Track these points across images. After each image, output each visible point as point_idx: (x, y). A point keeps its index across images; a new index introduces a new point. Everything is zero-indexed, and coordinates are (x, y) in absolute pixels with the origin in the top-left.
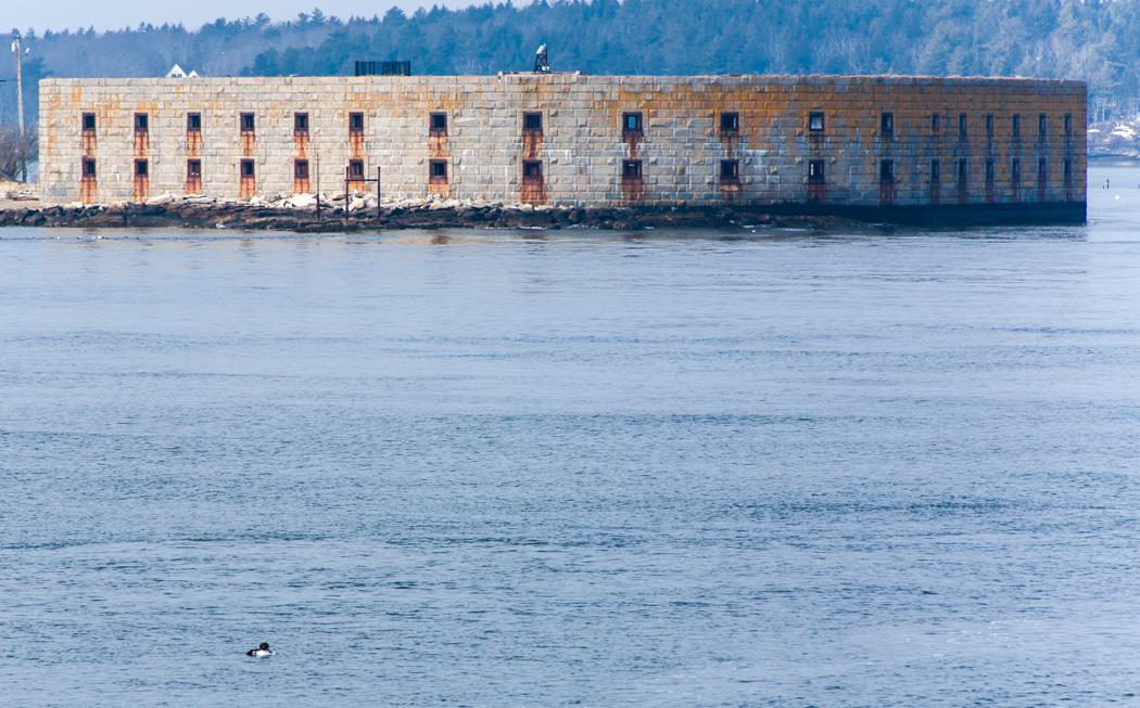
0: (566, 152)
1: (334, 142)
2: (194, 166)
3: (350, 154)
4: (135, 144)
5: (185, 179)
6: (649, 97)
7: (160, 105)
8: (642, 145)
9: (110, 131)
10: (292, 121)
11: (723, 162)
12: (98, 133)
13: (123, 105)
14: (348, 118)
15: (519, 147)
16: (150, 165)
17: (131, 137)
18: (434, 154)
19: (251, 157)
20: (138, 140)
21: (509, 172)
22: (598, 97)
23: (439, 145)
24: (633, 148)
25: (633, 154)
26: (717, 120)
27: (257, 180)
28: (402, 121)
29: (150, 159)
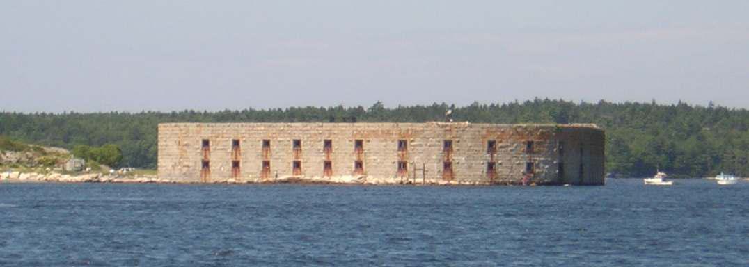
1: (346, 153)
2: (266, 164)
3: (355, 158)
5: (261, 169)
8: (495, 155)
9: (218, 148)
10: (322, 143)
11: (489, 163)
13: (225, 136)
17: (230, 150)
19: (299, 160)
20: (234, 152)
21: (436, 166)
25: (492, 159)
28: (384, 143)
29: (241, 161)
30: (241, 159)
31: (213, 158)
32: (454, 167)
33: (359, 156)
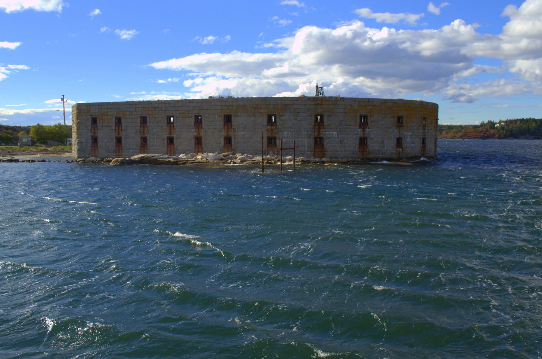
0: (334, 133)
3: (224, 134)
4: (115, 130)
6: (371, 108)
7: (127, 113)
8: (367, 130)
12: (98, 126)
14: (223, 117)
15: (312, 131)
16: (123, 139)
17: (114, 127)
18: (269, 134)
20: (117, 128)
22: (349, 107)
23: (272, 130)
24: (363, 131)
25: (364, 134)
26: (396, 118)
27: (175, 146)
29: (123, 137)
30: (123, 135)
31: (100, 135)
32: (325, 142)
33: (228, 132)
